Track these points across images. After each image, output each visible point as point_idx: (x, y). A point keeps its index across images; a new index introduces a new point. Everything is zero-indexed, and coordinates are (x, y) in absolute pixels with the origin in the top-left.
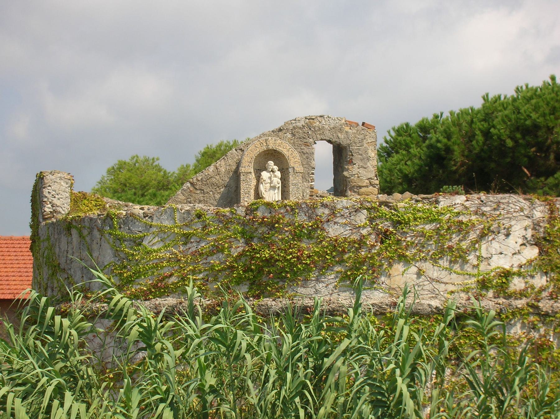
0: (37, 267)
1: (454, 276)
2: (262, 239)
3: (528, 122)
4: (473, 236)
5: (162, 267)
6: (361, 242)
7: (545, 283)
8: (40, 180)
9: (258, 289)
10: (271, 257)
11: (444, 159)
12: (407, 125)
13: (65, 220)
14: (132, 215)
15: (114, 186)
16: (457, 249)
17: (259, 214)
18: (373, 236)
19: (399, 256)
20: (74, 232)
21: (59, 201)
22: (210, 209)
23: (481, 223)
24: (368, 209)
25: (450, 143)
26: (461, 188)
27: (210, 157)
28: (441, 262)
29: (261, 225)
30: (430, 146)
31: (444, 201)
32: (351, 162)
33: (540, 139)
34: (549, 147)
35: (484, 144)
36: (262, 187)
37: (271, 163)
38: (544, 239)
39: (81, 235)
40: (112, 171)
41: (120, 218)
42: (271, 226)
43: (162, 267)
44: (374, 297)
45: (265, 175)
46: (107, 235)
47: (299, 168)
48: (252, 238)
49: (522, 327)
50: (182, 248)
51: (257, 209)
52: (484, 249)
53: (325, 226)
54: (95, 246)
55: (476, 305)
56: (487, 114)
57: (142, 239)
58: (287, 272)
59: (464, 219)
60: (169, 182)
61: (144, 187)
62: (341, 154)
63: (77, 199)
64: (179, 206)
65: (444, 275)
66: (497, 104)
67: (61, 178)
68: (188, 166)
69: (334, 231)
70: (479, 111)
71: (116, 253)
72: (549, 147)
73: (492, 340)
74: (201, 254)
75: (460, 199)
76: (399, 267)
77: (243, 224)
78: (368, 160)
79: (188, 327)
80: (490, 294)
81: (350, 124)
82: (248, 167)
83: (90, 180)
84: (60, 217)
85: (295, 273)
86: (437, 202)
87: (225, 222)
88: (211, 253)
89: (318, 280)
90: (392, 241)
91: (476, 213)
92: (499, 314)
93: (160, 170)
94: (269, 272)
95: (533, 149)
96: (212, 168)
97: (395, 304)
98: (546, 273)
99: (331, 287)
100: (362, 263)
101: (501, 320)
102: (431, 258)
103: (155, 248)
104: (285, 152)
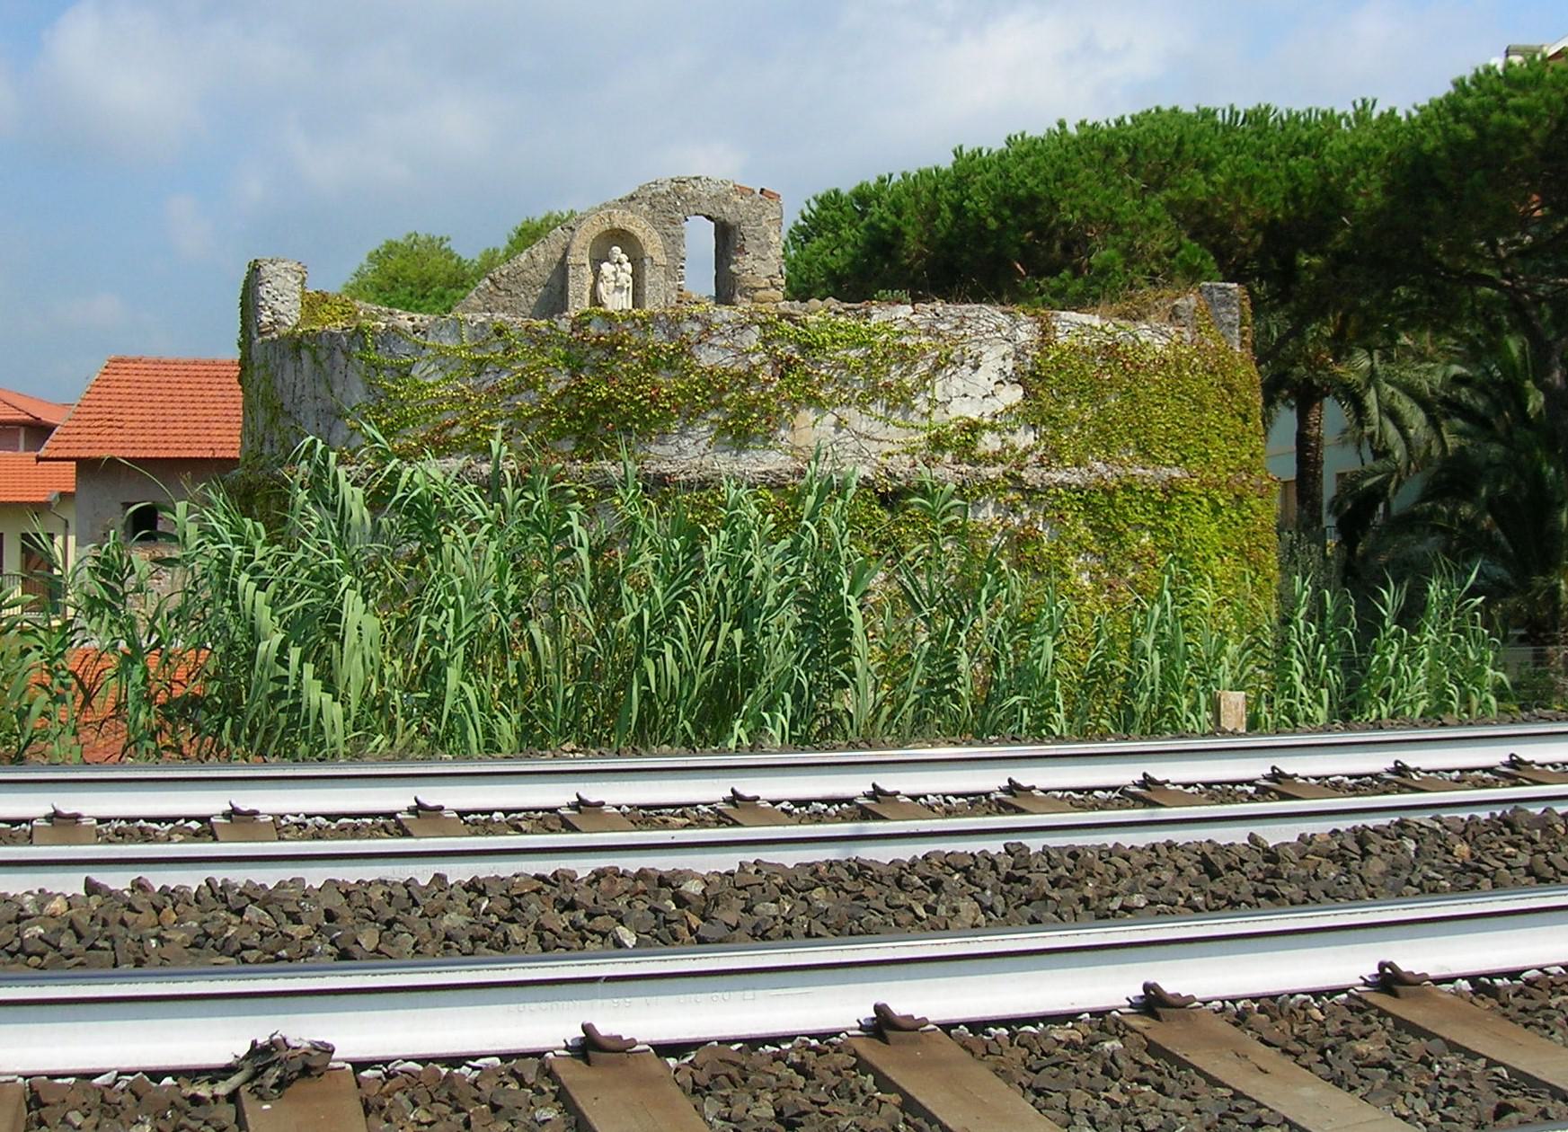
0: (249, 408)
1: (892, 429)
2: (597, 369)
3: (1021, 192)
4: (922, 368)
5: (441, 411)
6: (750, 376)
7: (1032, 442)
8: (255, 269)
9: (589, 446)
10: (610, 397)
11: (892, 247)
12: (836, 192)
13: (291, 336)
14: (395, 329)
15: (378, 280)
16: (898, 388)
17: (592, 330)
18: (769, 367)
19: (808, 398)
20: (305, 354)
21: (284, 306)
22: (517, 323)
23: (935, 348)
24: (762, 325)
25: (900, 223)
26: (903, 295)
27: (529, 235)
28: (872, 407)
29: (596, 348)
30: (871, 227)
31: (879, 315)
32: (742, 250)
33: (1039, 219)
34: (1054, 231)
35: (954, 224)
36: (602, 287)
37: (617, 249)
38: (1032, 374)
39: (315, 361)
40: (376, 257)
41: (375, 334)
42: (611, 349)
43: (441, 411)
44: (773, 461)
45: (607, 268)
46: (356, 361)
47: (661, 259)
48: (581, 368)
49: (995, 510)
50: (472, 381)
51: (588, 323)
52: (939, 388)
53: (695, 350)
54: (337, 377)
55: (926, 475)
56: (959, 179)
57: (410, 366)
58: (635, 421)
59: (910, 342)
60: (465, 275)
61: (426, 283)
62: (727, 238)
63: (313, 303)
64: (469, 317)
65: (877, 429)
66: (974, 163)
67: (286, 270)
68: (495, 251)
69: (709, 358)
70: (947, 173)
71: (370, 388)
72: (1054, 231)
73: (950, 527)
74: (502, 392)
75: (904, 311)
76: (808, 415)
77: (569, 345)
78: (769, 247)
79: (473, 505)
80: (948, 457)
81: (741, 191)
82: (580, 256)
83: (336, 274)
84: (283, 330)
85: (647, 423)
86: (868, 315)
87: (540, 342)
88: (518, 390)
89: (682, 434)
90: (798, 374)
91: (928, 333)
92: (960, 489)
93: (452, 257)
94: (607, 421)
95: (1029, 234)
96: (524, 257)
97: (801, 473)
98: (1034, 427)
99: (703, 444)
100: (751, 409)
101: (964, 499)
102: (858, 402)
103: (431, 381)
104: (638, 233)
